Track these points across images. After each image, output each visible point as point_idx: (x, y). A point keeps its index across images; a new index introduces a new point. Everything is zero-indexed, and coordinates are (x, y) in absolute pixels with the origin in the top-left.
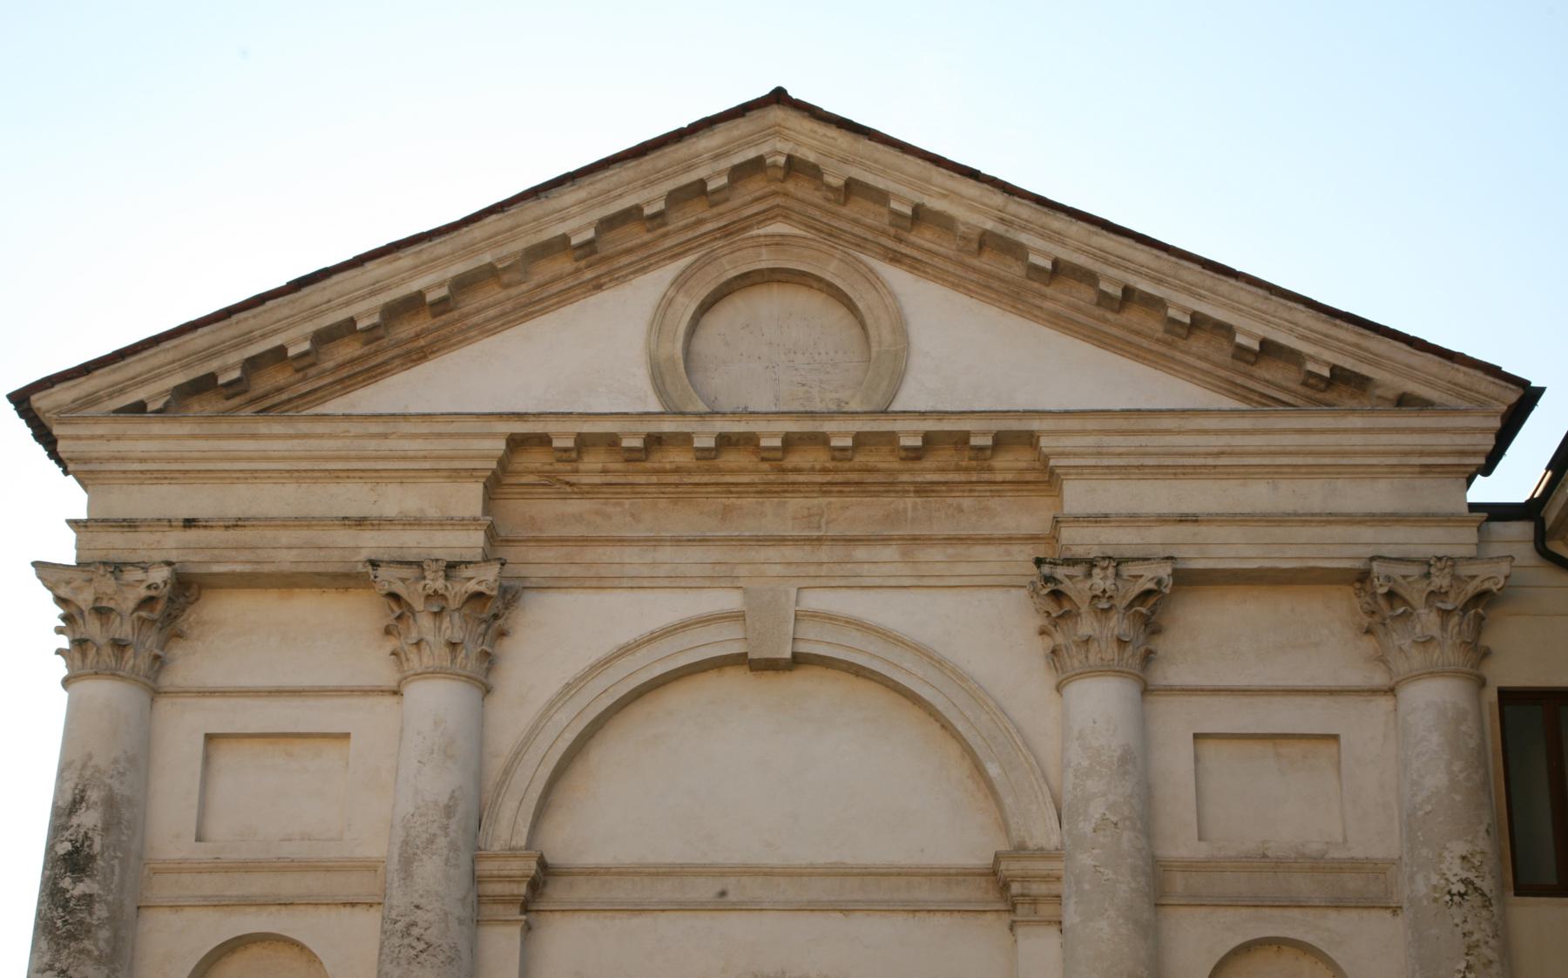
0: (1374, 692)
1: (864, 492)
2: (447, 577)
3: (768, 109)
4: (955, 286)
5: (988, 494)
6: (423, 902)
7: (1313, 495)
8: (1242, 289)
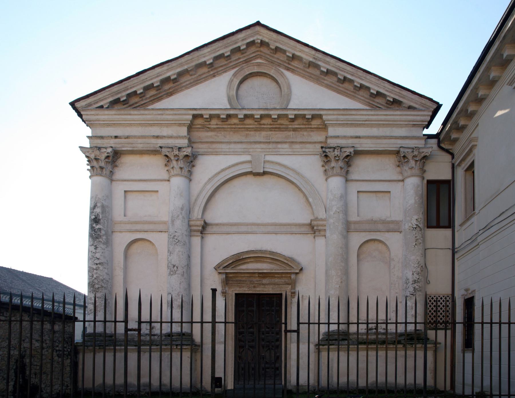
0: (399, 181)
2: (179, 151)
4: (303, 77)
6: (177, 231)
8: (373, 77)
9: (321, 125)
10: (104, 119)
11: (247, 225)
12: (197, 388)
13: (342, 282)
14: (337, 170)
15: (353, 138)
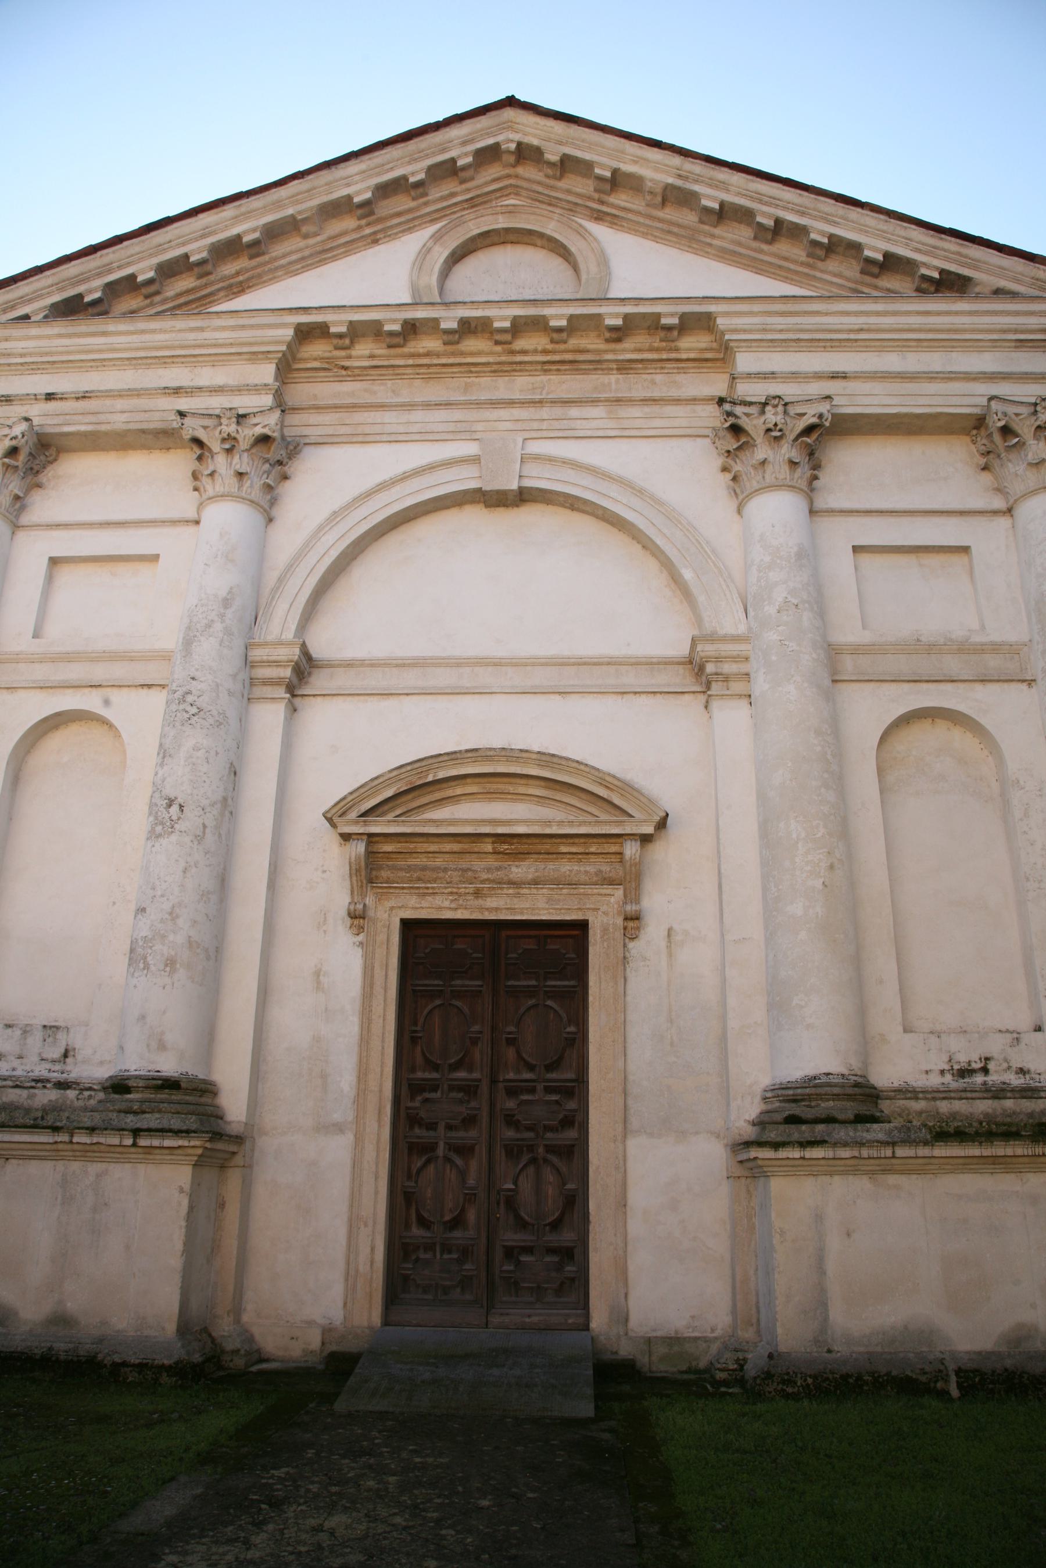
0: (995, 513)
1: (577, 370)
2: (238, 423)
3: (503, 110)
4: (645, 235)
5: (675, 371)
6: (197, 674)
7: (935, 361)
8: (867, 215)
9: (711, 349)
10: (25, 351)
11: (459, 665)
12: (213, 1340)
13: (831, 867)
14: (778, 470)
15: (820, 377)
